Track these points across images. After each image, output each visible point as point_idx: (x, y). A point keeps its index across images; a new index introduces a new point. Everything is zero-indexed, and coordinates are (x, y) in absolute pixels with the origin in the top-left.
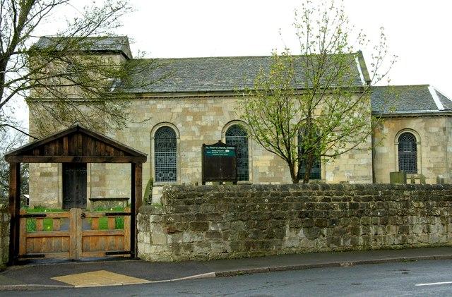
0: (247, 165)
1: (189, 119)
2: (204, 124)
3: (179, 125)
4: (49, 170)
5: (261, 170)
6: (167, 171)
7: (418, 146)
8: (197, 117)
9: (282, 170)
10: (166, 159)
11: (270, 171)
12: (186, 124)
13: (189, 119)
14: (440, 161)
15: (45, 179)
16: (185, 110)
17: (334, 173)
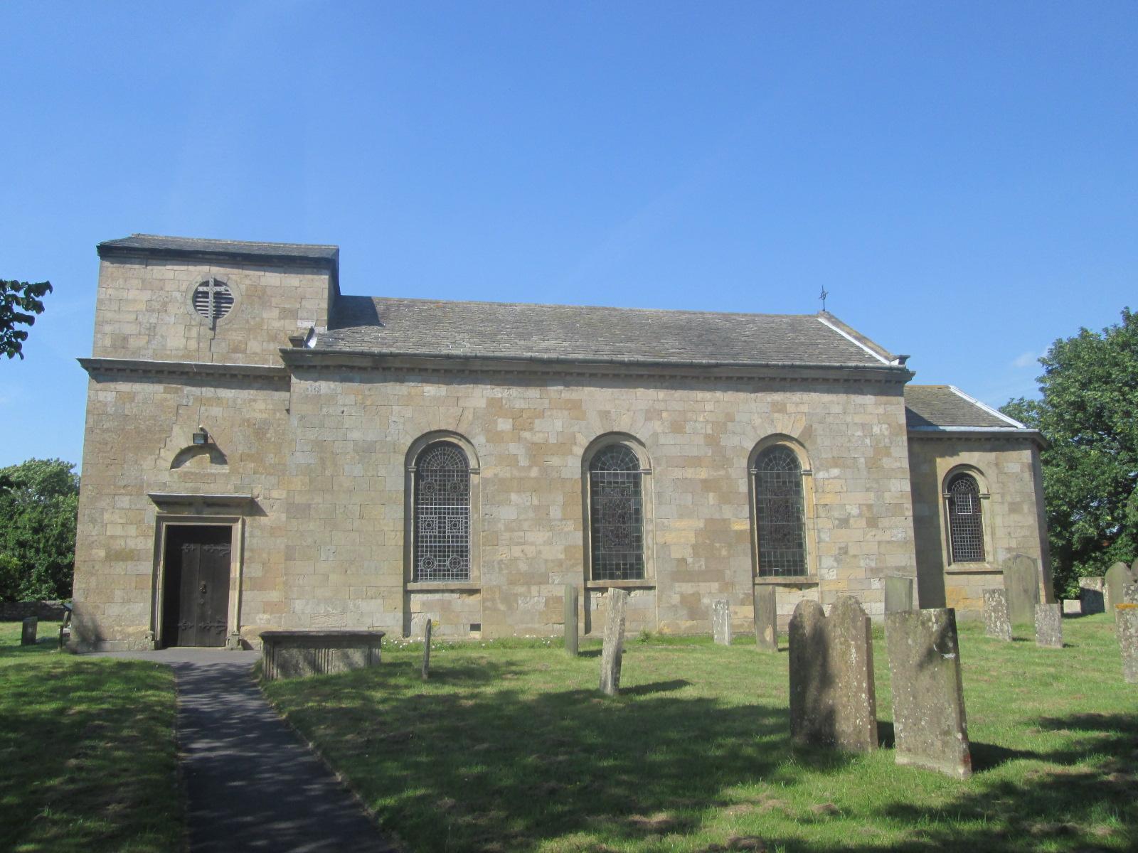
0: (639, 539)
1: (504, 425)
2: (538, 438)
3: (479, 440)
4: (131, 544)
5: (676, 554)
6: (443, 552)
7: (984, 503)
8: (522, 421)
9: (724, 553)
10: (441, 521)
11: (696, 554)
12: (495, 437)
13: (504, 425)
14: (1028, 533)
15: (119, 568)
16: (492, 402)
17: (838, 560)
